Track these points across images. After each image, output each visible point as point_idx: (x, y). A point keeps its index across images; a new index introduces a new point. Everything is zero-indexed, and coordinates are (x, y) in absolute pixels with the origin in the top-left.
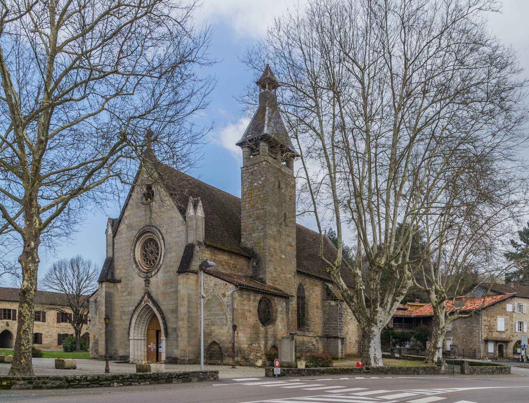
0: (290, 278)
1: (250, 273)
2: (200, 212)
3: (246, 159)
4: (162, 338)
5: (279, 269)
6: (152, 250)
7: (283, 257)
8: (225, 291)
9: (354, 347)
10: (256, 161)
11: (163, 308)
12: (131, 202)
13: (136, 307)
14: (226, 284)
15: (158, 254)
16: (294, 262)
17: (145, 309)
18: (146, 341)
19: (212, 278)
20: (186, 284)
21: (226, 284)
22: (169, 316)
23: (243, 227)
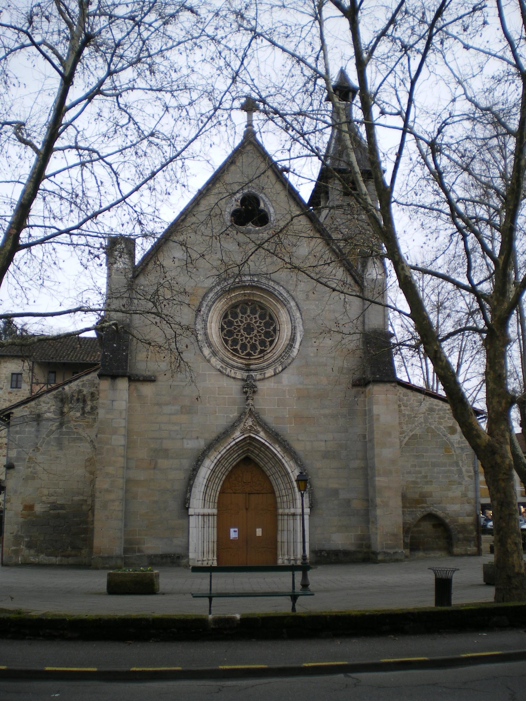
11: (298, 447)
12: (394, 158)
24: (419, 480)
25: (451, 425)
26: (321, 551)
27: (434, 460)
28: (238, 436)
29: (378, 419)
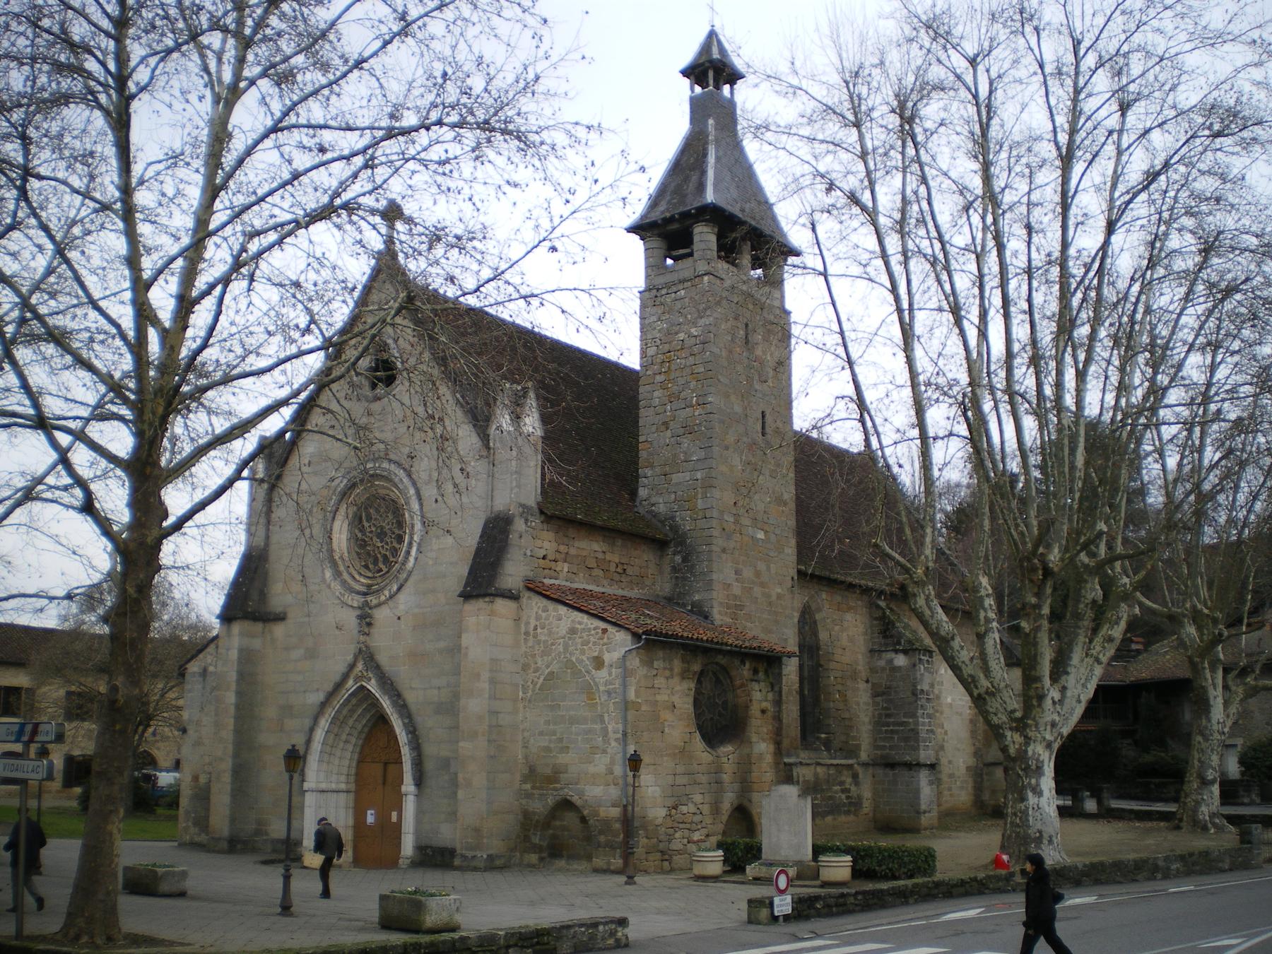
0: (779, 597)
1: (664, 586)
2: (532, 423)
3: (653, 268)
4: (404, 789)
5: (748, 573)
6: (382, 527)
7: (761, 535)
8: (601, 651)
9: (962, 788)
10: (687, 274)
11: (411, 697)
13: (331, 695)
14: (605, 631)
15: (400, 539)
16: (790, 551)
17: (354, 701)
18: (352, 796)
19: (563, 610)
20: (488, 631)
21: (605, 631)
22: (430, 724)
23: (643, 454)
24: (552, 745)
25: (596, 654)
26: (427, 847)
27: (572, 713)
28: (351, 685)
29: (466, 654)
